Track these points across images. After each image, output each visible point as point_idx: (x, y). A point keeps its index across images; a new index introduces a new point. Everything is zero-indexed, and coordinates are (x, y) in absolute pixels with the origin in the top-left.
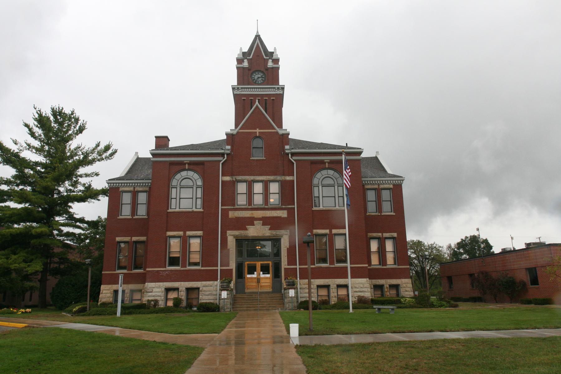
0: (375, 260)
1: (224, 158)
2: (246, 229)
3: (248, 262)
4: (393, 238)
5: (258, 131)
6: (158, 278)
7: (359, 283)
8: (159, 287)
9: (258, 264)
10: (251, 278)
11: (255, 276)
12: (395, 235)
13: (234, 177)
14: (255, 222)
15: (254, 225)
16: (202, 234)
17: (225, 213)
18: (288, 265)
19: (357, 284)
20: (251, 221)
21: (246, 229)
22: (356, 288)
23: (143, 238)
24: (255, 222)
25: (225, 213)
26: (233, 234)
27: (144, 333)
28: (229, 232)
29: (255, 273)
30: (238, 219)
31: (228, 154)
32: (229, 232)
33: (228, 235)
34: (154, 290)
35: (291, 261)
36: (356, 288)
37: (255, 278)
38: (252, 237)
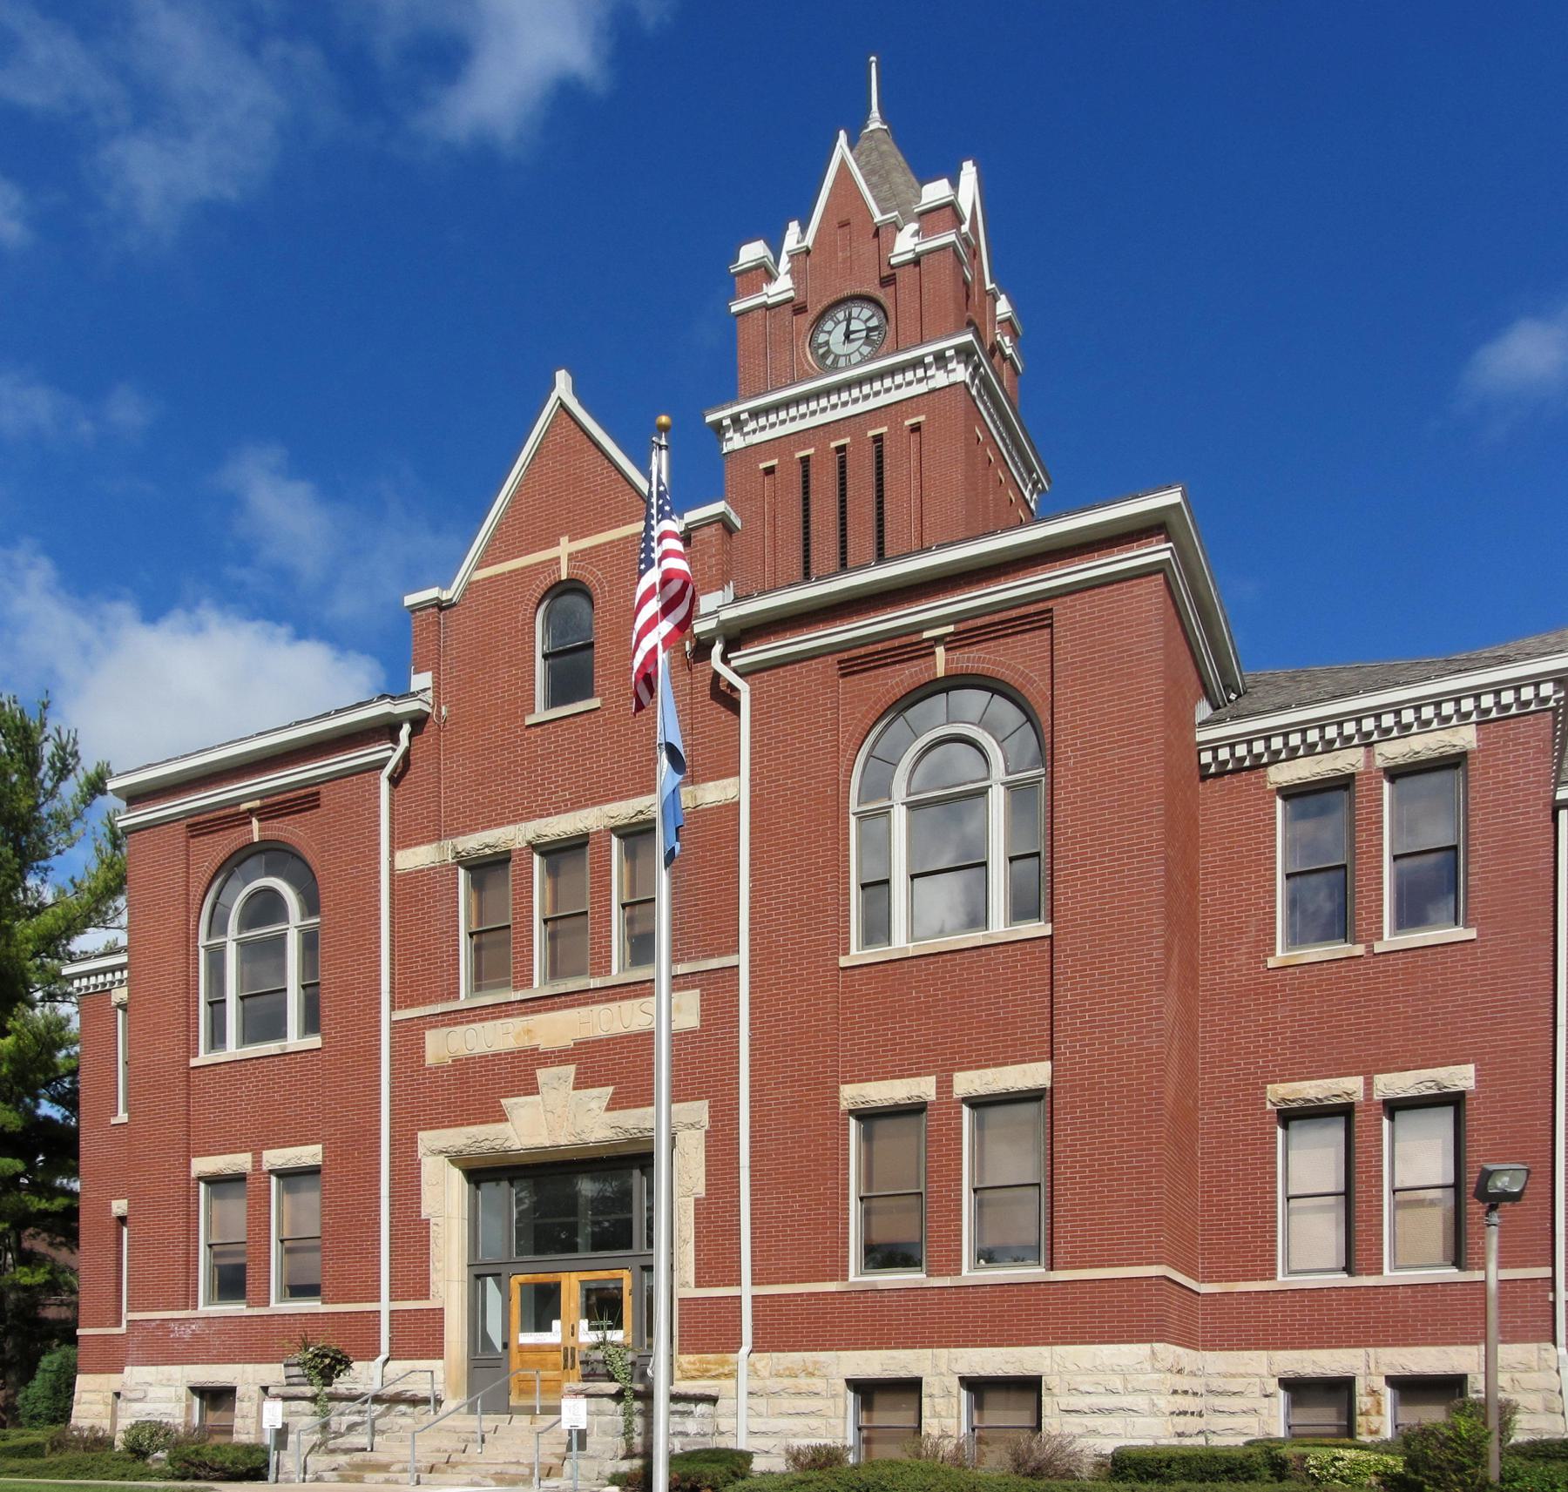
0: (1308, 1249)
1: (396, 741)
2: (502, 1117)
3: (521, 1278)
4: (1454, 1101)
5: (565, 548)
6: (161, 1348)
7: (1094, 1370)
8: (168, 1383)
9: (572, 1287)
10: (537, 1349)
11: (555, 1335)
12: (1462, 1077)
13: (448, 844)
14: (543, 1075)
15: (534, 1090)
16: (318, 1160)
17: (409, 1037)
18: (698, 1285)
19: (1089, 1372)
20: (518, 1072)
21: (502, 1117)
22: (1073, 1390)
23: (1036, 1074)
24: (543, 1075)
25: (409, 1037)
26: (440, 1145)
27: (819, 301)
28: (427, 1140)
29: (556, 1324)
30: (465, 1068)
31: (419, 722)
32: (427, 1140)
33: (421, 1150)
34: (154, 1392)
35: (716, 1261)
36: (1073, 1390)
37: (554, 1348)
38: (531, 1151)
